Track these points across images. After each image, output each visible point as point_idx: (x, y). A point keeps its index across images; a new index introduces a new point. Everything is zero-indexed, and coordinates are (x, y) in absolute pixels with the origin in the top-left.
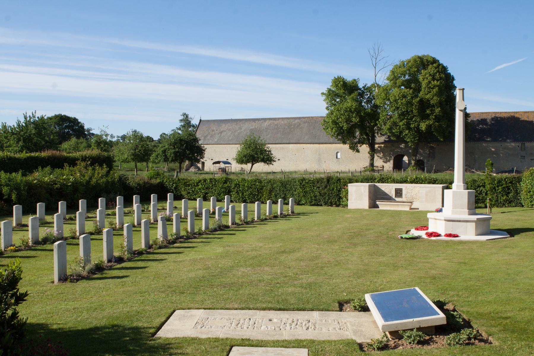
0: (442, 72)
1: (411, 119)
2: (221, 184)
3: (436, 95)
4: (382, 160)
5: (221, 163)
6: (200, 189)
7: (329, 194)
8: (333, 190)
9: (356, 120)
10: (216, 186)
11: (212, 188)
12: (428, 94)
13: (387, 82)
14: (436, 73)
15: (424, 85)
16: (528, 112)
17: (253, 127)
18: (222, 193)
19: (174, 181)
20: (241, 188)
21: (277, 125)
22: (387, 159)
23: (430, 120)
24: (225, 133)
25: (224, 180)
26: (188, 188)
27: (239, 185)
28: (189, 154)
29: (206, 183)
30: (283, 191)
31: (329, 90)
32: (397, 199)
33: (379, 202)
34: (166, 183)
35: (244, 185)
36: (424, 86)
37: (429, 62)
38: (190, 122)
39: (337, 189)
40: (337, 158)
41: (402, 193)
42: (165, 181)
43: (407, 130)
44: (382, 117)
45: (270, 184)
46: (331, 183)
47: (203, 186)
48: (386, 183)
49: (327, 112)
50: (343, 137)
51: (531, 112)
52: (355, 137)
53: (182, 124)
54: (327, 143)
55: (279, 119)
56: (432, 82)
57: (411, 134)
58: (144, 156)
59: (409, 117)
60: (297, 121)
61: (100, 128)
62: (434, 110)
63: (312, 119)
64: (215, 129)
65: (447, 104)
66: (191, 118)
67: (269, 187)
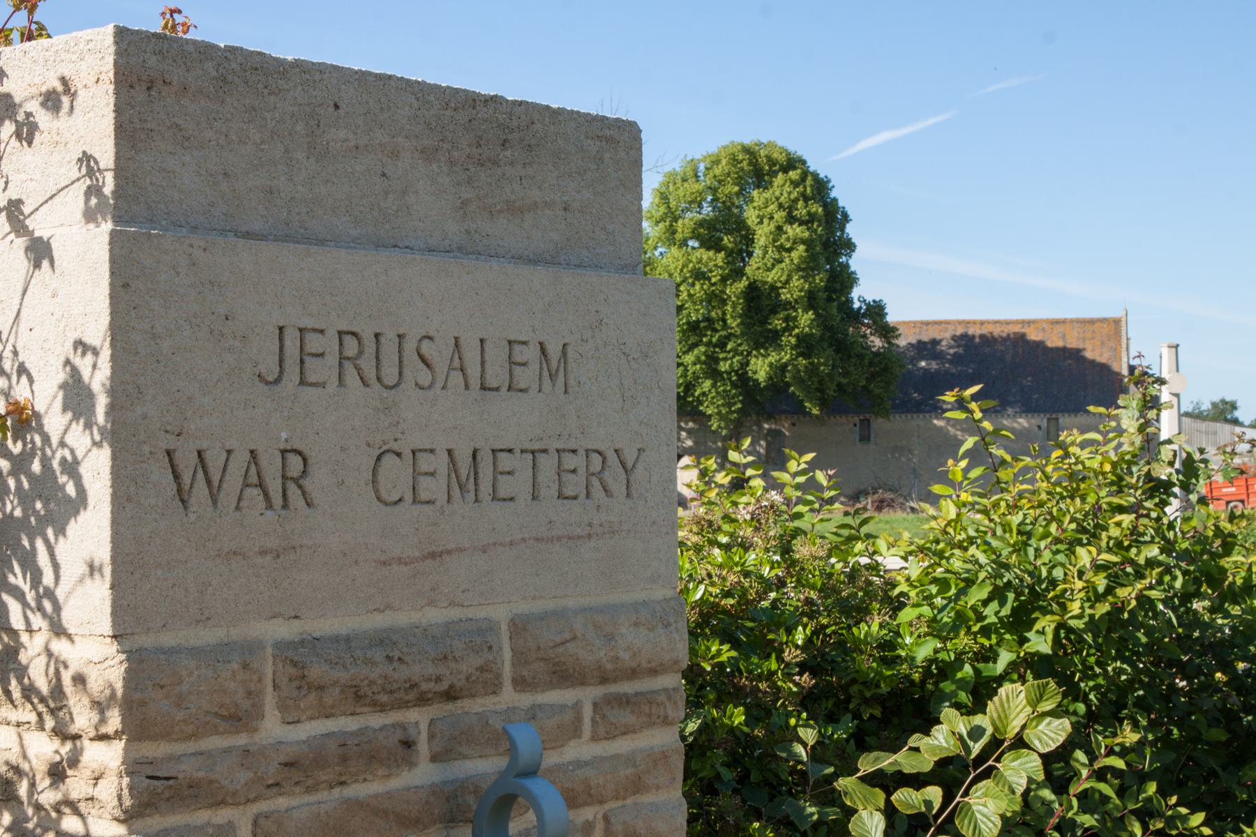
1: (722, 344)
14: (796, 201)
15: (762, 235)
23: (780, 348)
51: (1072, 321)
57: (718, 393)
59: (714, 340)
62: (795, 319)
65: (830, 299)
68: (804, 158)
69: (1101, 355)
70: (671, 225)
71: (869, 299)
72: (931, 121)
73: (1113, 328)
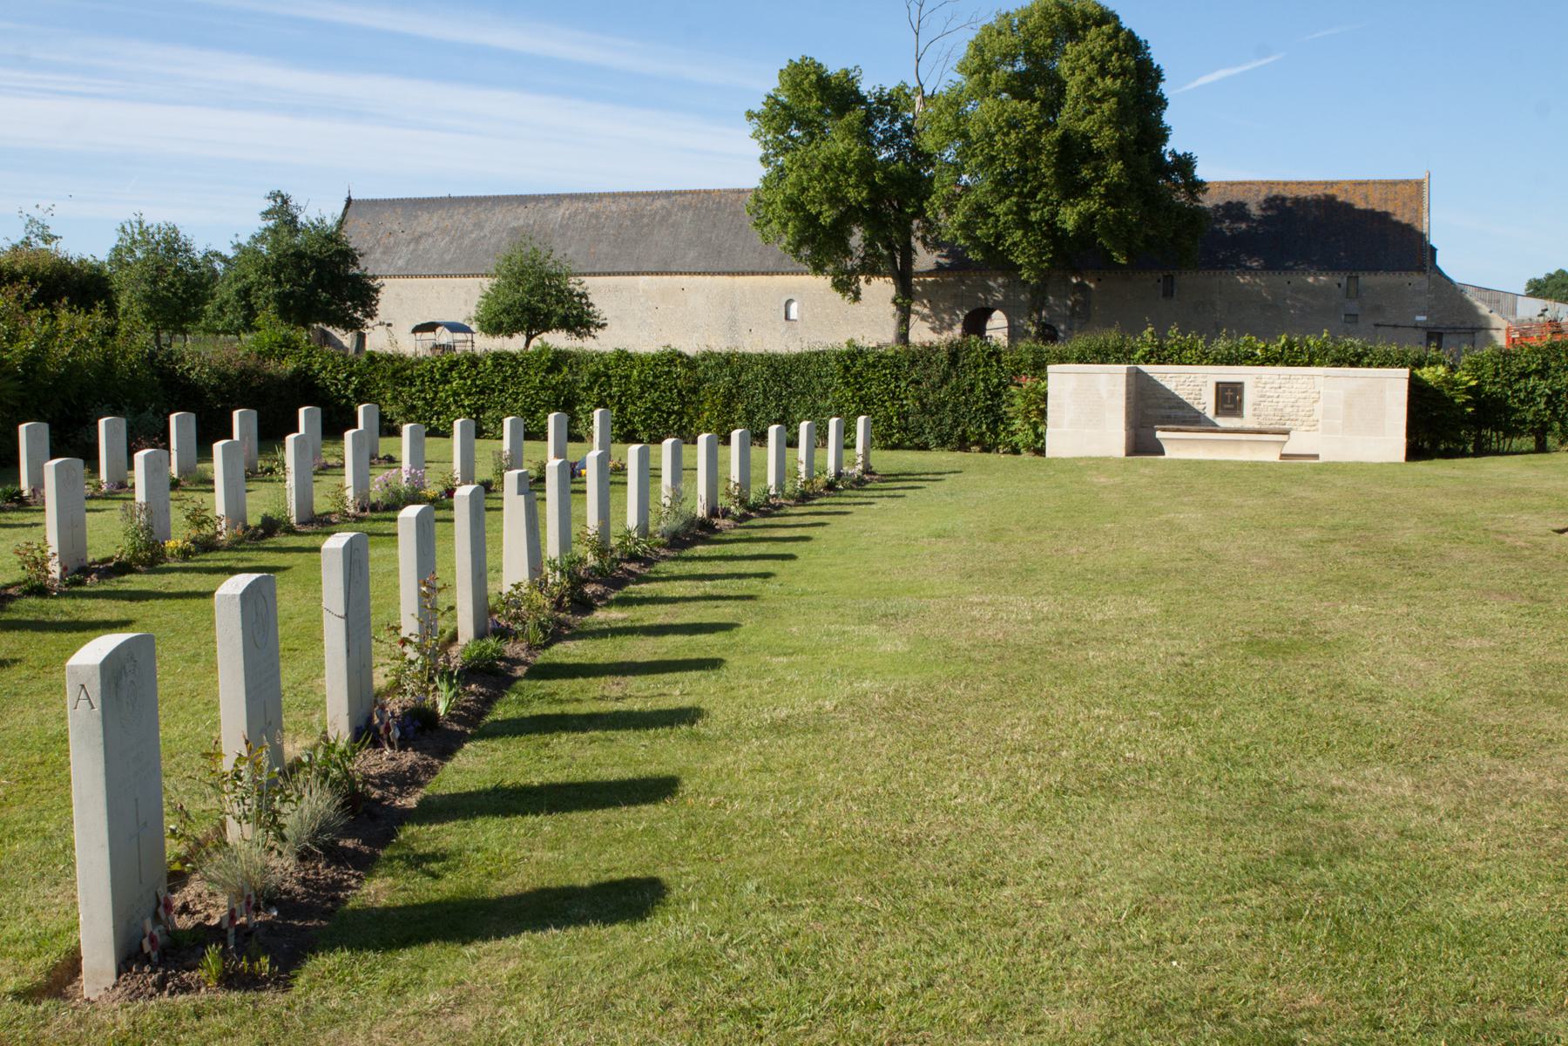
0: (1126, 52)
1: (1032, 194)
2: (536, 374)
3: (1110, 121)
4: (928, 325)
5: (439, 330)
6: (455, 394)
7: (955, 405)
8: (972, 390)
9: (859, 194)
10: (520, 383)
11: (501, 391)
12: (1084, 117)
13: (958, 77)
14: (1110, 54)
15: (1073, 89)
16: (1366, 183)
17: (521, 222)
18: (540, 407)
19: (351, 366)
20: (615, 389)
21: (596, 216)
22: (942, 321)
23: (1091, 197)
24: (430, 240)
25: (549, 360)
26: (407, 389)
27: (609, 377)
28: (329, 303)
29: (478, 373)
30: (779, 396)
31: (773, 100)
32: (1223, 422)
33: (1164, 430)
34: (323, 374)
35: (628, 377)
36: (1073, 94)
37: (1088, 19)
38: (294, 219)
39: (987, 387)
40: (787, 318)
41: (1241, 401)
42: (316, 367)
43: (1018, 228)
44: (941, 190)
45: (726, 371)
46: (964, 365)
47: (469, 382)
48: (1172, 363)
49: (763, 171)
50: (815, 252)
51: (1374, 182)
52: (848, 252)
53: (271, 223)
54: (758, 274)
55: (601, 196)
56: (1098, 80)
57: (1028, 242)
58: (185, 303)
59: (1025, 190)
60: (658, 203)
61: (25, 212)
62: (1104, 169)
63: (706, 196)
64: (396, 227)
65: (1140, 153)
66: (299, 208)
67: (725, 382)
68: (1117, 13)
69: (1403, 215)
70: (985, 77)
71: (1180, 152)
72: (1222, 74)
73: (1417, 189)
